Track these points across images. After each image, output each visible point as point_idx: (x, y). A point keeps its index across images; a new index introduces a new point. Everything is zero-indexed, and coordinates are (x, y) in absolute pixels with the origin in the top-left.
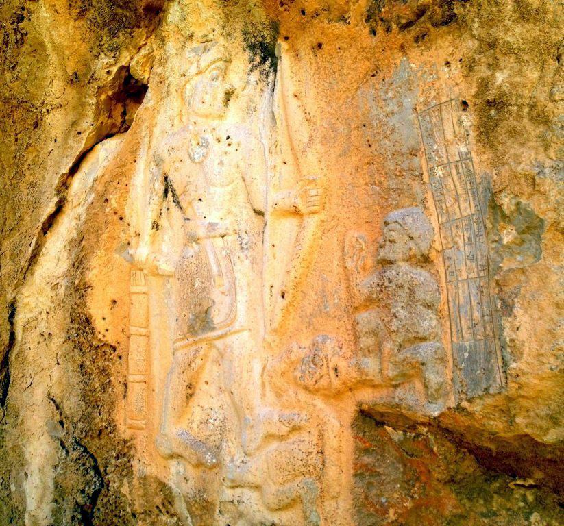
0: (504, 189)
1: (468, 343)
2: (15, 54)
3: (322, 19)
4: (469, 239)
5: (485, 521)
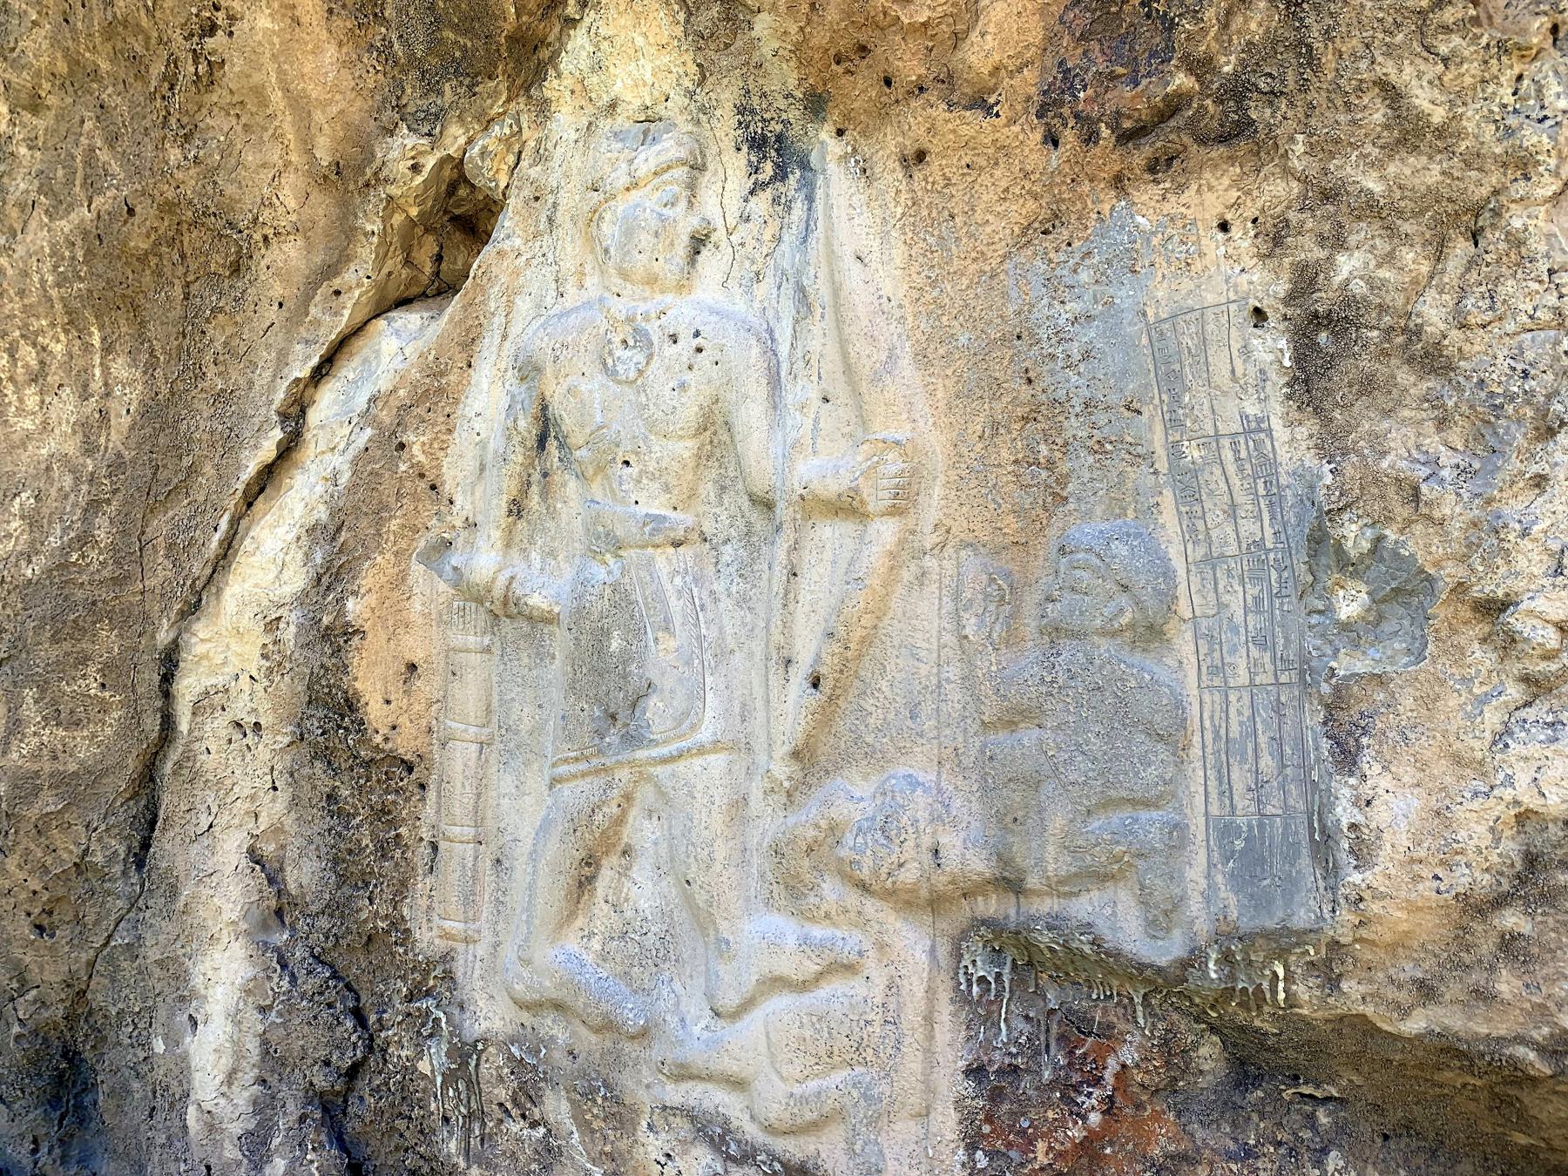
0: (1348, 506)
2: (192, 107)
3: (933, 99)
5: (1234, 1167)
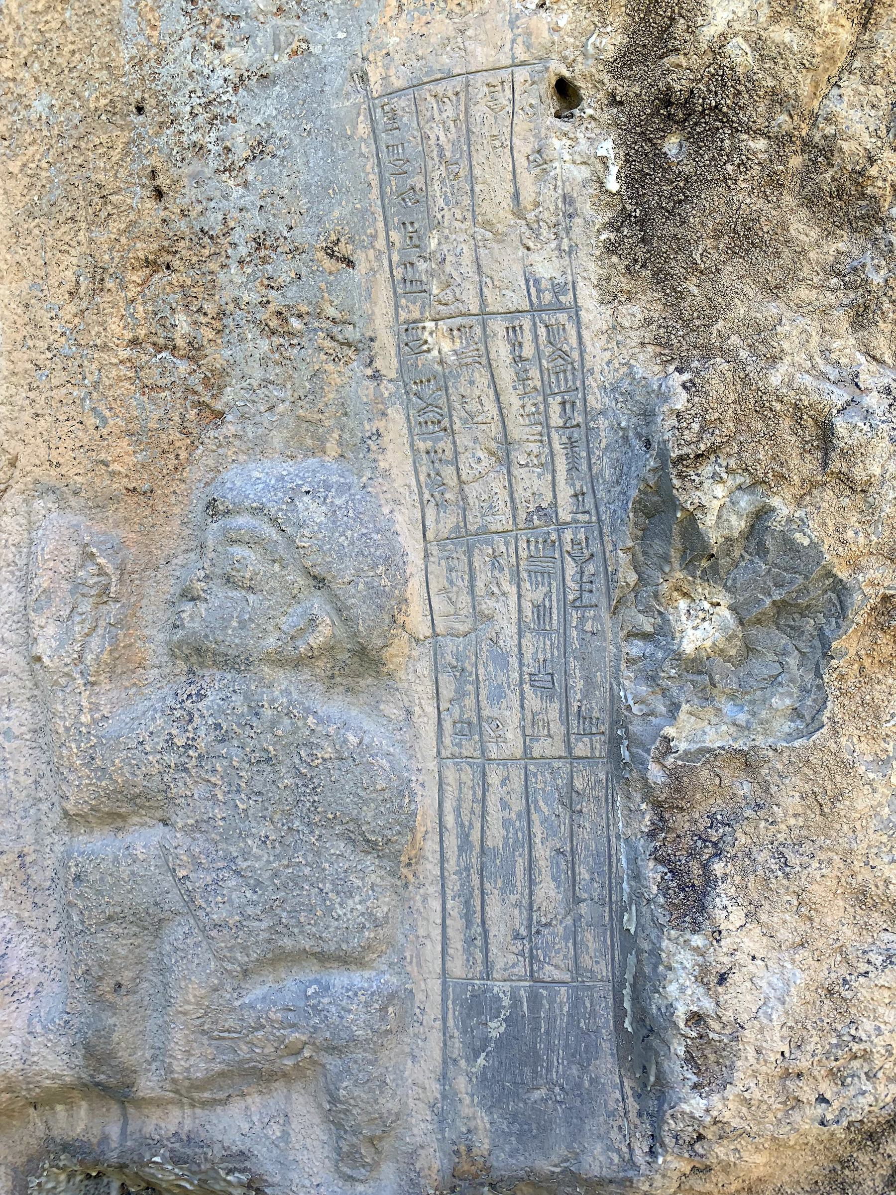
0: (714, 450)
1: (507, 986)
4: (542, 612)
